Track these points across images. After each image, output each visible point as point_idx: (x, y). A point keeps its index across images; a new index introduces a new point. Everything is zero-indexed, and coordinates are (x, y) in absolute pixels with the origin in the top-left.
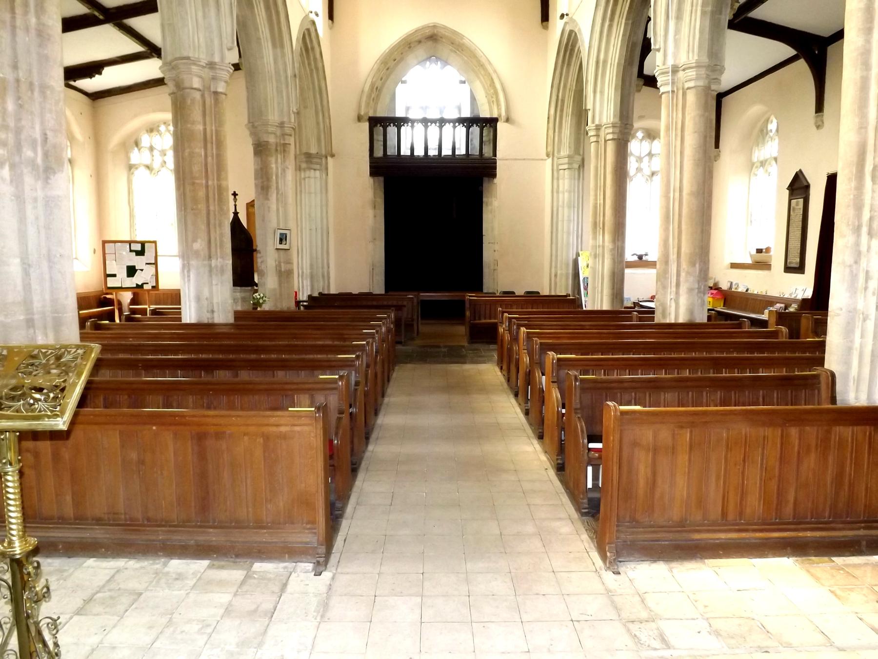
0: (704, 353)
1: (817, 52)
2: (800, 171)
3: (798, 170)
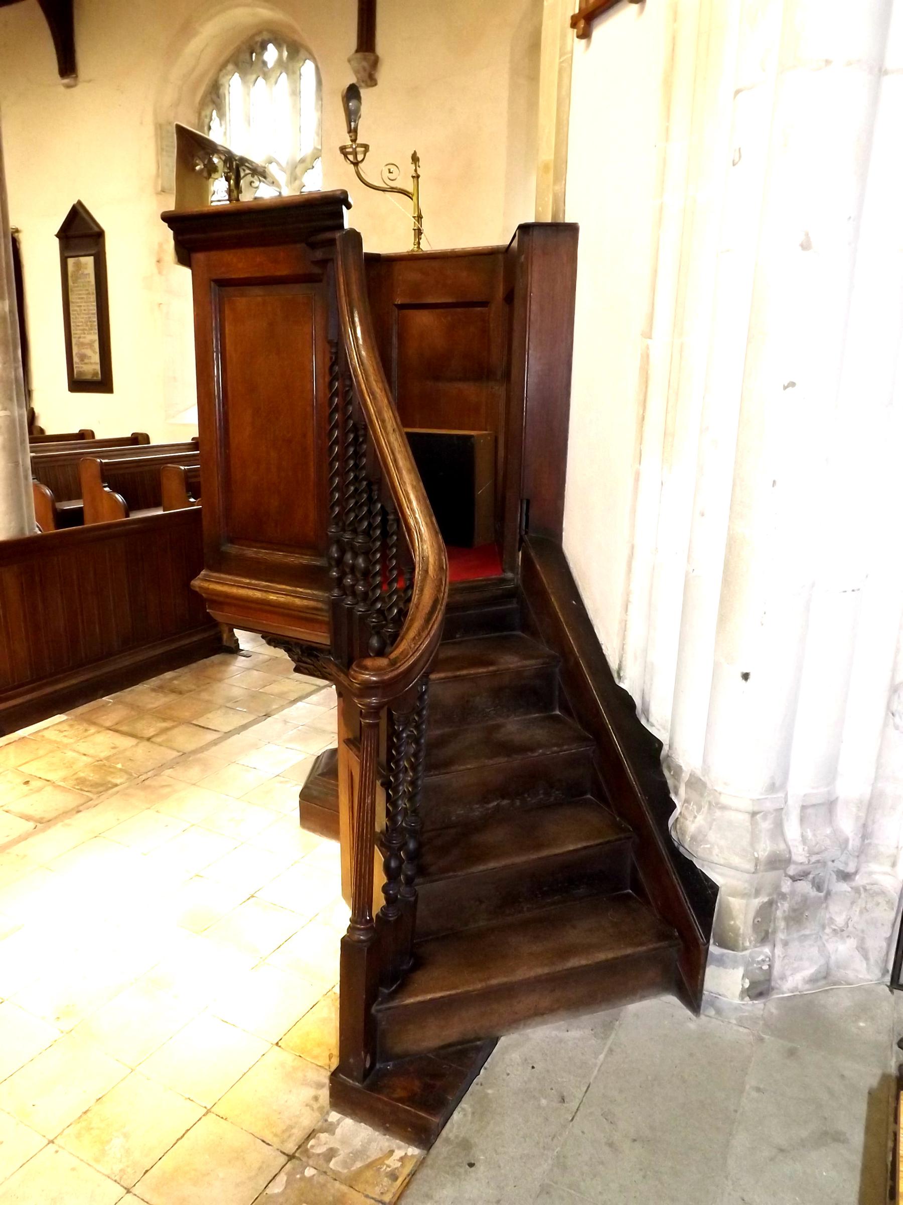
0: (774, 1011)
1: (391, 892)
2: (79, 203)
3: (75, 202)
